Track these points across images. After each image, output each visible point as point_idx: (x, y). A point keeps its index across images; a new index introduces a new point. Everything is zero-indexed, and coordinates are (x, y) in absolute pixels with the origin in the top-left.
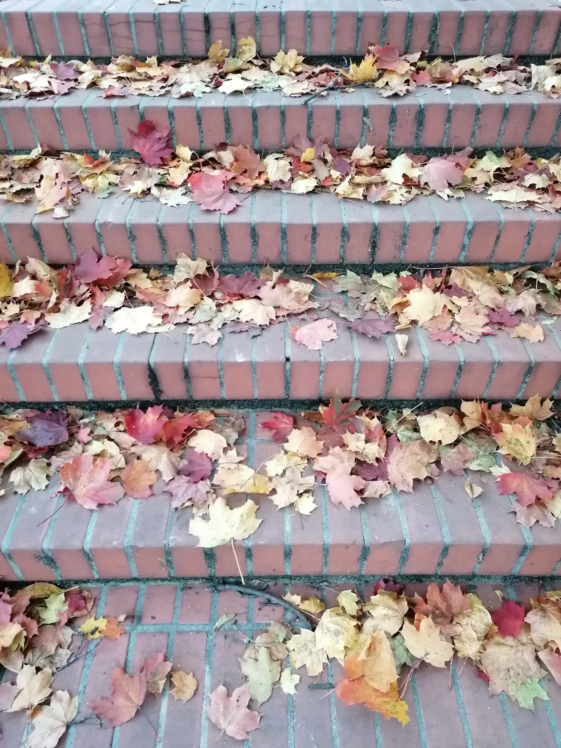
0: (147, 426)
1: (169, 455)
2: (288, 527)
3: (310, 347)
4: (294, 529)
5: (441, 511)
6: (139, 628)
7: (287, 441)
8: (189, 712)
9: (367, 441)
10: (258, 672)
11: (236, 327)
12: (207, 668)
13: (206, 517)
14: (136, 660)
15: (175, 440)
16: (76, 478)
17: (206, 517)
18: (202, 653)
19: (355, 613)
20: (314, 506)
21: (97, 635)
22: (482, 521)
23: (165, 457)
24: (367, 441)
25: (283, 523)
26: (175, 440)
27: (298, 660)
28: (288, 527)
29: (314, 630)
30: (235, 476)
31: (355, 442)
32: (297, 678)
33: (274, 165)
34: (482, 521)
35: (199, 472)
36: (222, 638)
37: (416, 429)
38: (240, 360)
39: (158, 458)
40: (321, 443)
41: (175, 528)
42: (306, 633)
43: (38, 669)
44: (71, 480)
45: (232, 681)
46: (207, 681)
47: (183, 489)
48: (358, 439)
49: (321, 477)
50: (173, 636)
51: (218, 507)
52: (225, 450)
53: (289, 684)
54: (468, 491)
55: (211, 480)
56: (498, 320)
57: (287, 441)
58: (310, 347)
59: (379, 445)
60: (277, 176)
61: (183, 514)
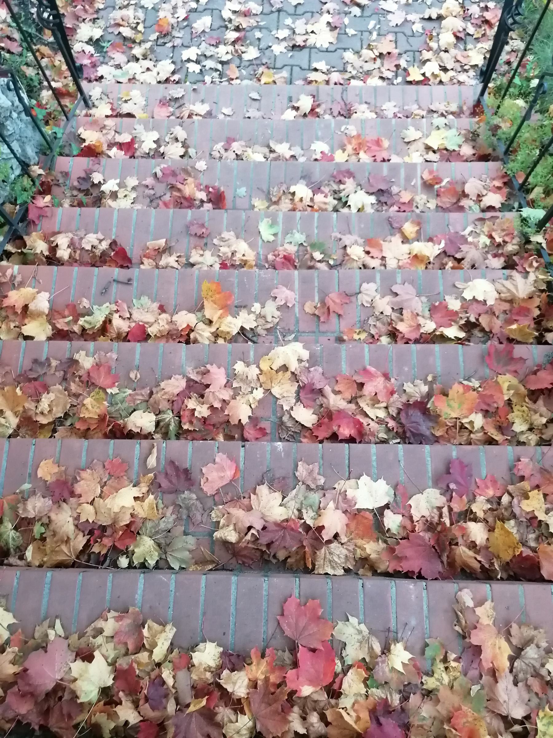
0: (348, 427)
1: (329, 404)
2: (252, 353)
3: (225, 456)
4: (249, 352)
5: (160, 363)
6: (336, 335)
7: (249, 417)
8: (305, 297)
9: (195, 409)
10: (271, 310)
11: (283, 485)
12: (297, 315)
13: (300, 361)
14: (334, 318)
15: (327, 416)
16: (385, 387)
17: (300, 361)
18: (300, 322)
19: (220, 338)
20: (234, 367)
21: (358, 331)
22: (137, 356)
23: (332, 402)
24: (195, 409)
25: (254, 356)
26: (327, 416)
27: (252, 317)
28: (252, 353)
29: (242, 327)
30: (284, 390)
31: (202, 411)
32: (253, 309)
33: (240, 687)
34: (137, 356)
35: (308, 393)
36: (291, 329)
37: (158, 424)
38: (280, 443)
39: (336, 402)
40: (226, 413)
41: (318, 354)
42: (247, 327)
43: (382, 313)
44: (388, 385)
45: (284, 308)
46: (297, 310)
47: (316, 376)
48: (200, 412)
49: (229, 384)
50: (317, 331)
51: (294, 366)
52: (292, 408)
53: (257, 307)
54: (139, 376)
55: (299, 385)
56: (63, 491)
57: (249, 417)
58: (225, 456)
59: (187, 406)
60: (237, 676)
61: (313, 361)
